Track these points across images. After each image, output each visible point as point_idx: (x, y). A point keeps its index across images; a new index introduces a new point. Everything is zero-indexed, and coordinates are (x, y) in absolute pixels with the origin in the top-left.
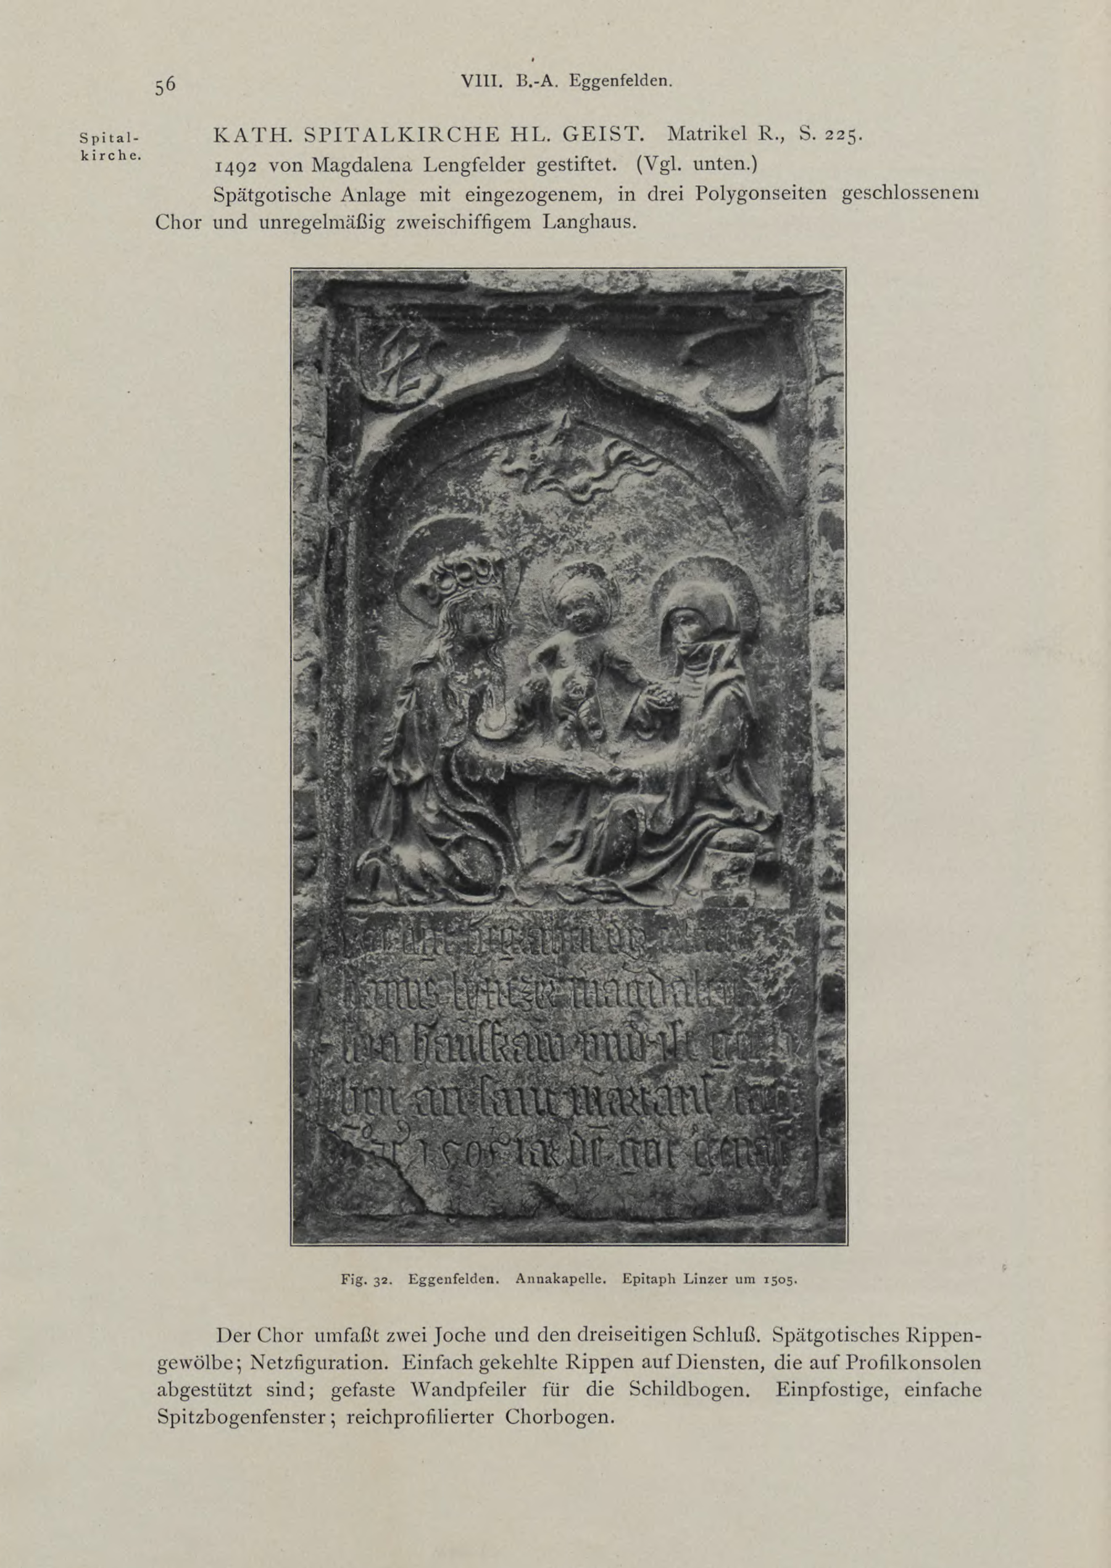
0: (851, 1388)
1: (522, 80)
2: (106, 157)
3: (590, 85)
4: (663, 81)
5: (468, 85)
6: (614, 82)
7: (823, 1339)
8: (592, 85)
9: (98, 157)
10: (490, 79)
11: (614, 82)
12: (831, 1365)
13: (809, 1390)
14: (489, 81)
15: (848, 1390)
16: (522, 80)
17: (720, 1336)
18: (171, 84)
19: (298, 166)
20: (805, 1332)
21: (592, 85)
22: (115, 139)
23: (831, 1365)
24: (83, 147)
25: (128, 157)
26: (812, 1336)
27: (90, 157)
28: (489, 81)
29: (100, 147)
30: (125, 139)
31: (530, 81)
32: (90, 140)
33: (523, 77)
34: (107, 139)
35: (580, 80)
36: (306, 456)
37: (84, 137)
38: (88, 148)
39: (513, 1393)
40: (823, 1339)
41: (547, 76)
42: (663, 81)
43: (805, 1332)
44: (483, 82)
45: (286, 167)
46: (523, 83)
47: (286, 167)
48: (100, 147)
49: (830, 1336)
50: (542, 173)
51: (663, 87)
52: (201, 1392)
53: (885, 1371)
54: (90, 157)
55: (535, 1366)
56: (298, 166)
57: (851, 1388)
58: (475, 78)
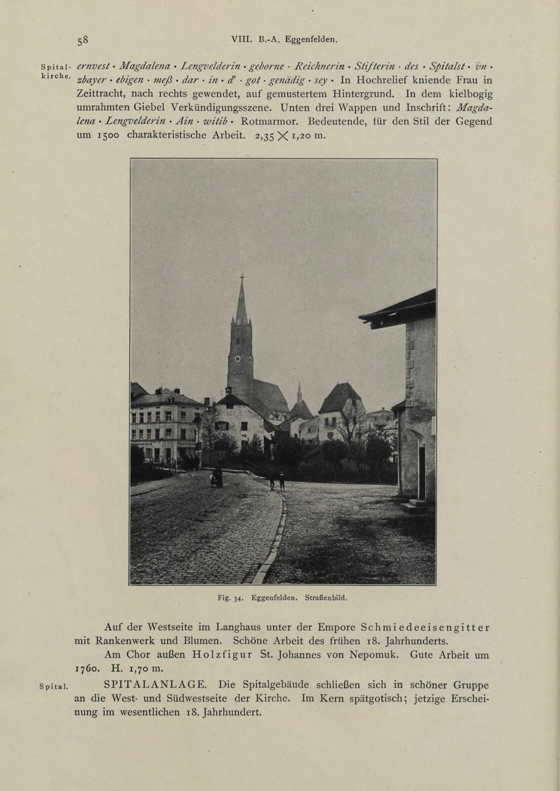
0: (180, 134)
1: (261, 39)
2: (54, 77)
3: (296, 41)
4: (332, 40)
5: (235, 41)
6: (308, 40)
7: (374, 700)
8: (296, 41)
9: (50, 77)
10: (246, 38)
11: (308, 40)
12: (118, 628)
13: (334, 628)
14: (246, 39)
15: (179, 135)
16: (261, 39)
17: (329, 685)
18: (86, 40)
19: (341, 655)
20: (365, 697)
21: (296, 41)
22: (59, 68)
23: (118, 628)
24: (43, 71)
25: (64, 77)
26: (368, 699)
27: (46, 77)
28: (246, 39)
29: (51, 72)
30: (64, 68)
31: (265, 39)
32: (47, 68)
33: (262, 38)
34: (55, 68)
35: (291, 39)
36: (210, 423)
37: (43, 67)
38: (45, 72)
39: (243, 700)
40: (374, 700)
41: (274, 37)
42: (332, 40)
43: (365, 697)
44: (242, 40)
45: (335, 655)
46: (262, 40)
47: (335, 655)
48: (51, 72)
49: (377, 699)
50: (269, 98)
51: (332, 43)
52: (127, 699)
53: (378, 659)
54: (46, 77)
55: (332, 686)
56: (341, 655)
57: (180, 134)
58: (238, 38)
